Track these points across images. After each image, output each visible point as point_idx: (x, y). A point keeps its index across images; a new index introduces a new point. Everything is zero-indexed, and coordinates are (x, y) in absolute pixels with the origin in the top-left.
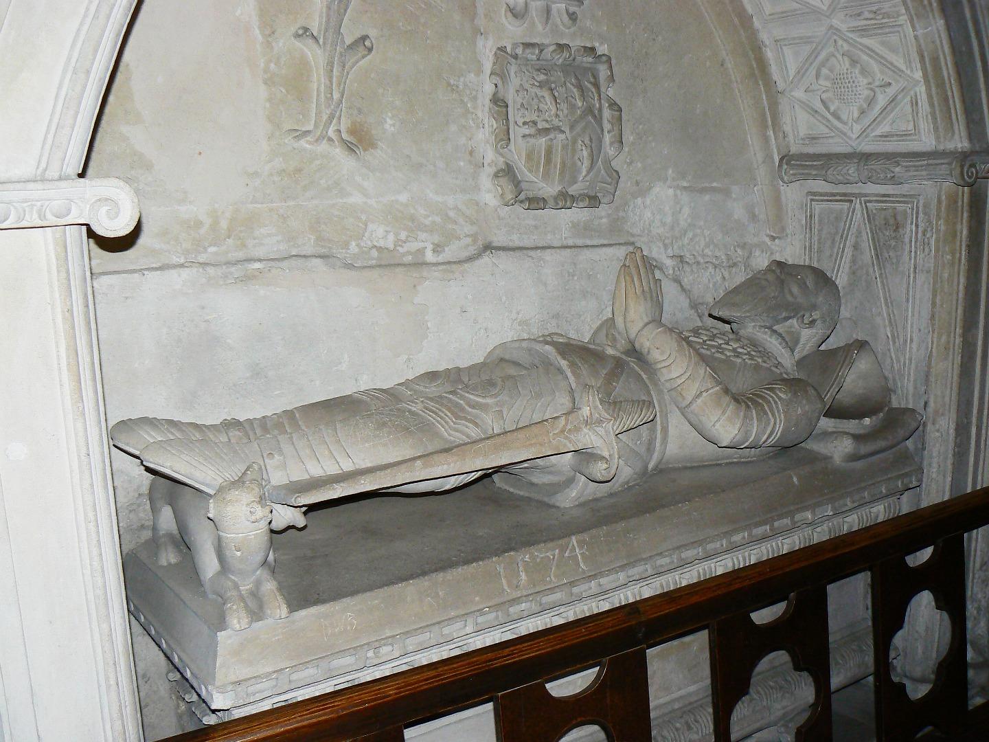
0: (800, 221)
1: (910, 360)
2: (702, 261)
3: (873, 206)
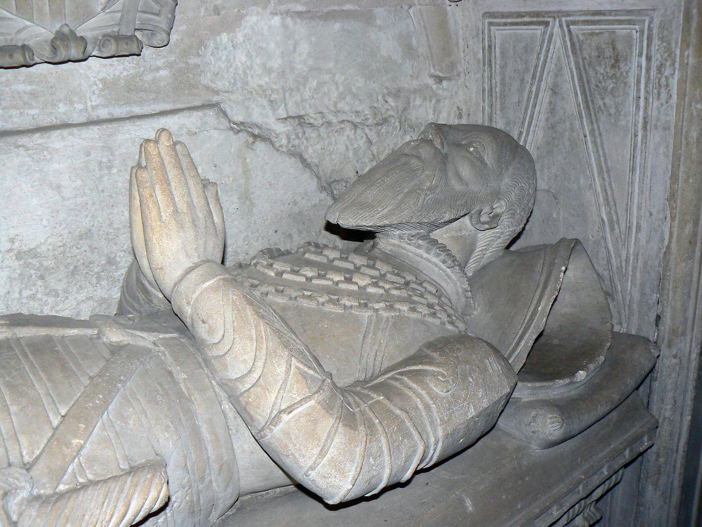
0: (475, 54)
1: (636, 255)
2: (335, 121)
3: (579, 30)
